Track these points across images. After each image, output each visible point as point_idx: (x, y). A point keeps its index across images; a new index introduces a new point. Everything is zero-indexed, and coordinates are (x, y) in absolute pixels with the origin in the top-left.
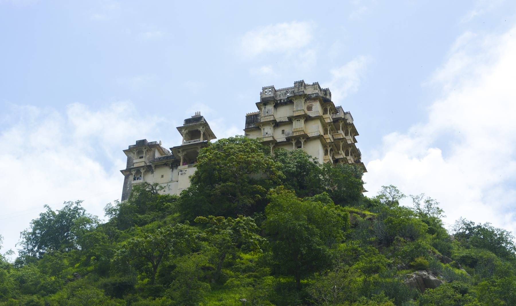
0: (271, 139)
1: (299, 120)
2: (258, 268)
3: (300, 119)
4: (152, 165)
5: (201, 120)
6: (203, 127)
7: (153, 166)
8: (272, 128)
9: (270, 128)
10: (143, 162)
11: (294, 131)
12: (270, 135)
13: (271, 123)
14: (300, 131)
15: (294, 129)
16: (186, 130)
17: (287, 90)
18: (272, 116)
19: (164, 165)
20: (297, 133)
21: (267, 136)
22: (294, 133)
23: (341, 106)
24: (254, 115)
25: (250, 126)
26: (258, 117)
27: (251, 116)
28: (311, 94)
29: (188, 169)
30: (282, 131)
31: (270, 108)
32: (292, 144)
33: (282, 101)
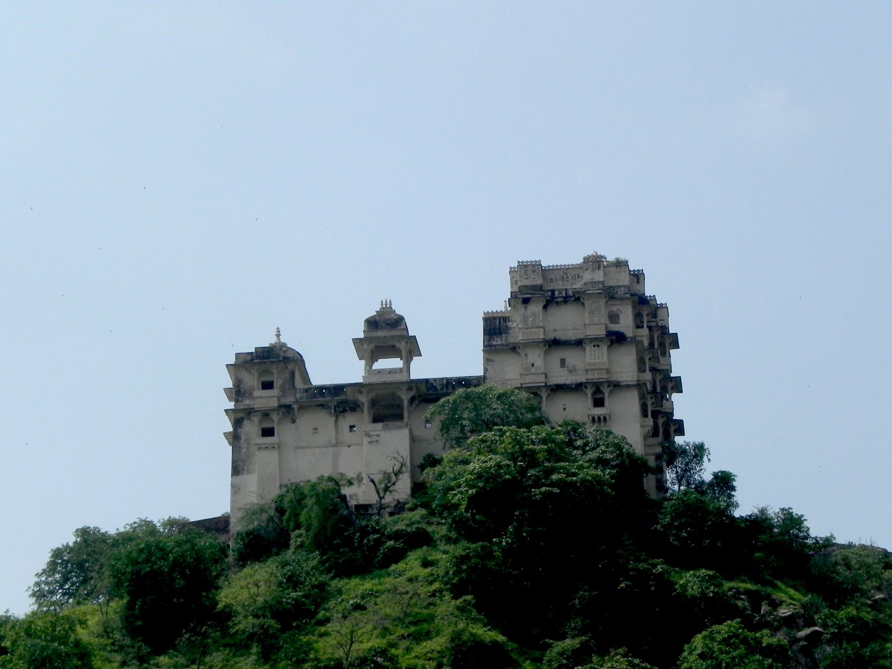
0: (544, 384)
1: (598, 346)
2: (408, 526)
3: (599, 343)
4: (293, 405)
5: (400, 325)
6: (407, 343)
7: (295, 407)
8: (542, 353)
9: (539, 355)
10: (274, 397)
11: (590, 367)
12: (540, 369)
13: (541, 345)
14: (601, 369)
15: (589, 364)
16: (370, 343)
17: (565, 271)
18: (542, 330)
19: (319, 405)
20: (594, 374)
21: (533, 370)
22: (589, 372)
23: (666, 304)
24: (500, 318)
25: (494, 341)
26: (509, 322)
27: (495, 318)
28: (615, 287)
29: (382, 433)
30: (561, 360)
31: (536, 308)
32: (586, 395)
33: (556, 293)
